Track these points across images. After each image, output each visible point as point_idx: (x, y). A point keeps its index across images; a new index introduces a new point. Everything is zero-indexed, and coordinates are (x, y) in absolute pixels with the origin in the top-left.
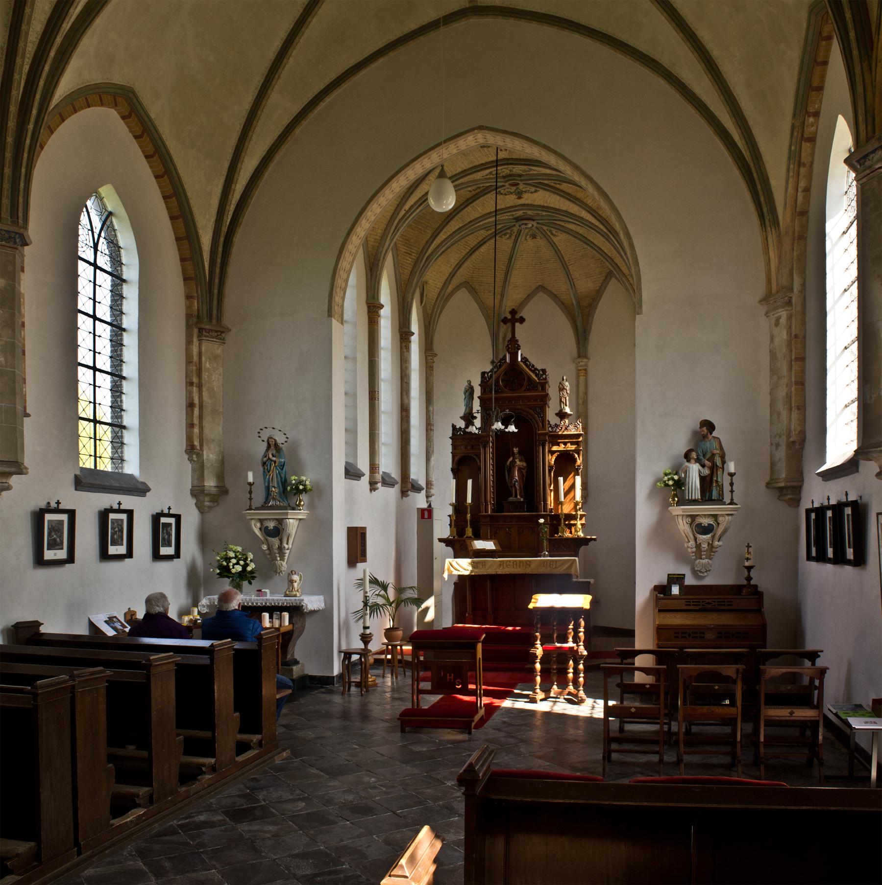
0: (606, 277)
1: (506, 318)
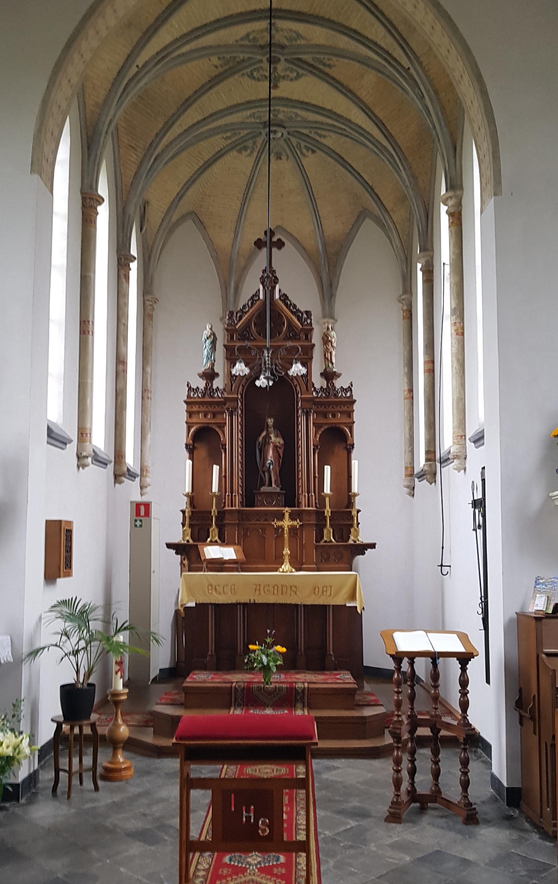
0: (358, 217)
1: (259, 240)
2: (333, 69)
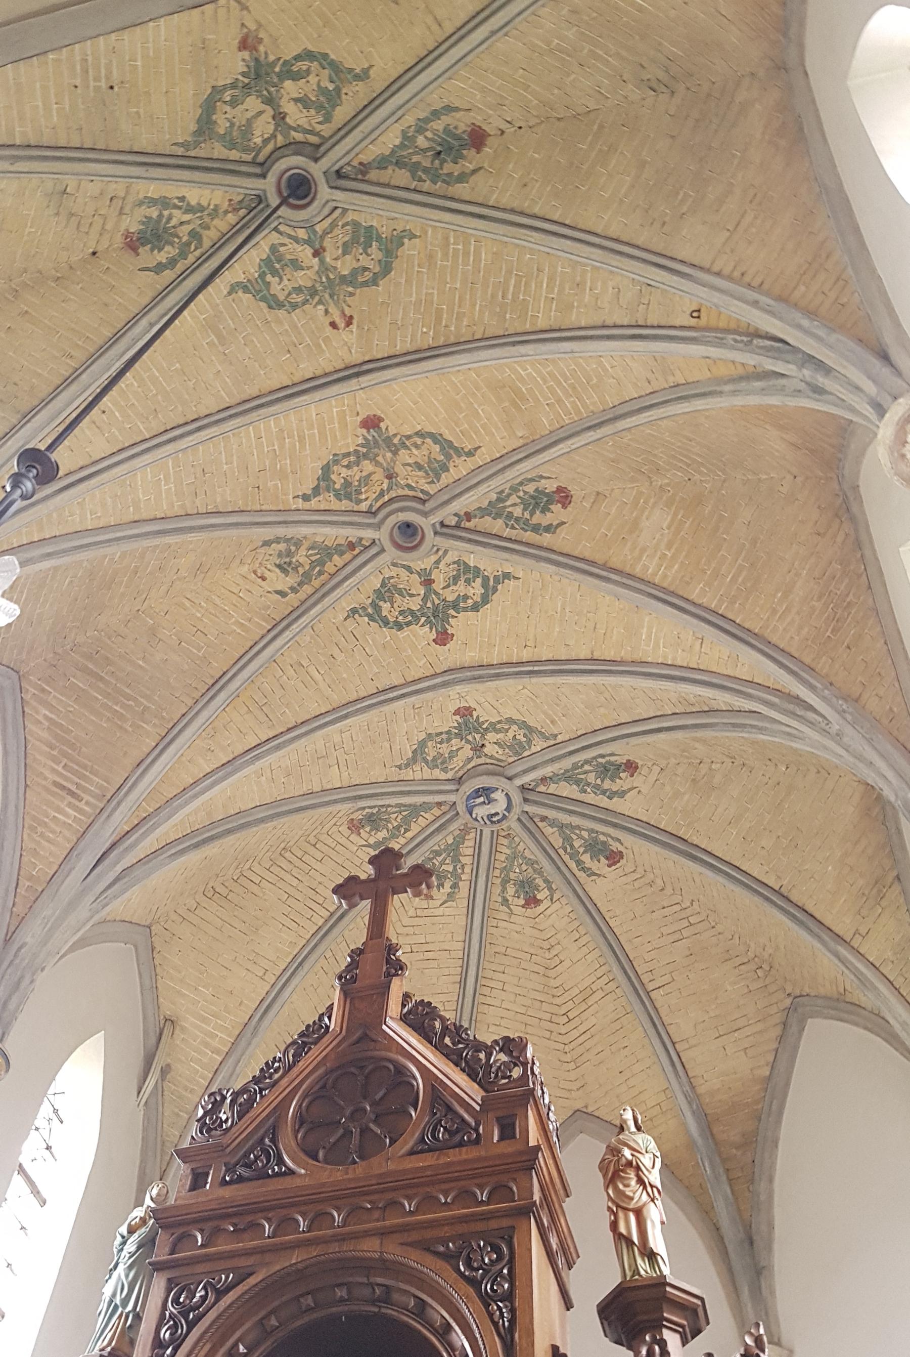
2: (562, 532)
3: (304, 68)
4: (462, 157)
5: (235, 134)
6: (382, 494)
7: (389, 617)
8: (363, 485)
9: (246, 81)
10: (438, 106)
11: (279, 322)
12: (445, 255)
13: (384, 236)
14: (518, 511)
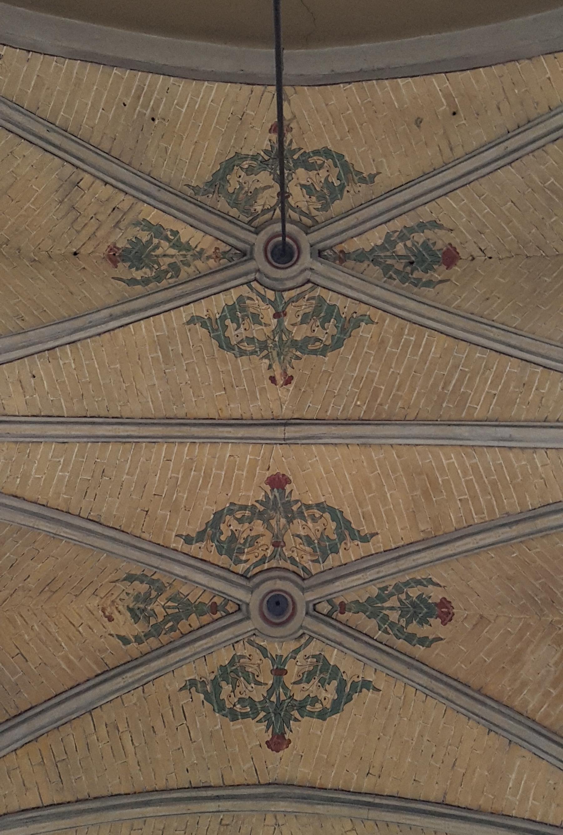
2: (437, 648)
3: (319, 162)
4: (432, 269)
5: (241, 196)
6: (263, 560)
7: (227, 702)
8: (248, 545)
9: (266, 158)
10: (425, 219)
11: (224, 361)
12: (397, 344)
13: (343, 316)
14: (394, 616)
